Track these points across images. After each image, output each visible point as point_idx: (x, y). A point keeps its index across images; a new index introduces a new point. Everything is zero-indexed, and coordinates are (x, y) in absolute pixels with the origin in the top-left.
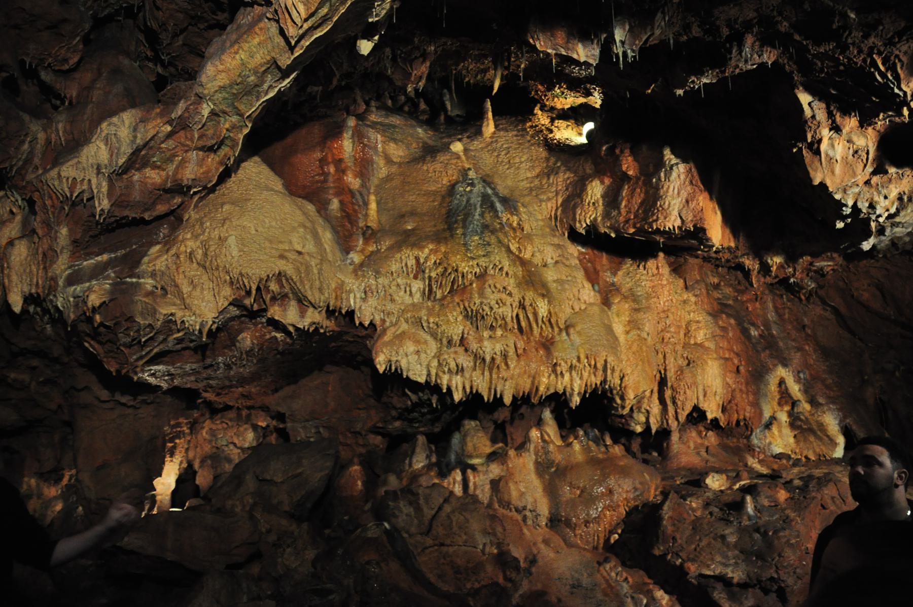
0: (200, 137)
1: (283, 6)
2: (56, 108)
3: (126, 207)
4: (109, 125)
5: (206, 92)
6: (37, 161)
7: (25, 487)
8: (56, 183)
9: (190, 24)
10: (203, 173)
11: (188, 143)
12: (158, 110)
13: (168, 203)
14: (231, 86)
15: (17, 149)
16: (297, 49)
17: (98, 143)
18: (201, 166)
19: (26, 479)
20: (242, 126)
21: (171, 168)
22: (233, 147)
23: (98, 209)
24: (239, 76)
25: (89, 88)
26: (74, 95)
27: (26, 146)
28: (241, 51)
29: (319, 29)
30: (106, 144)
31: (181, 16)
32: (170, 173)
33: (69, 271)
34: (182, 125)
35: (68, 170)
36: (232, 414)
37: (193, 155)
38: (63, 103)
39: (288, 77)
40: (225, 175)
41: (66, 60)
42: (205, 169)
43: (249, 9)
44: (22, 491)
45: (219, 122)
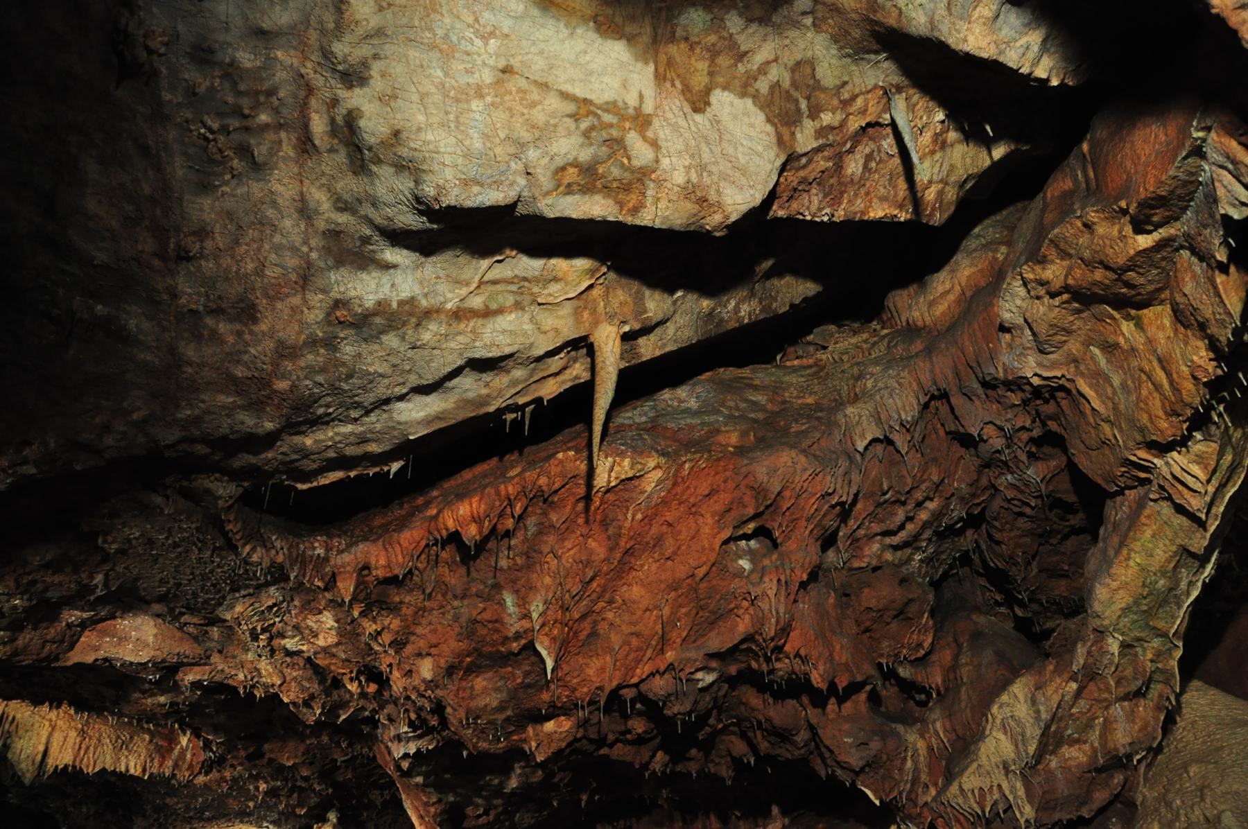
0: (1118, 683)
1: (1169, 477)
2: (923, 704)
3: (1054, 809)
4: (1000, 707)
5: (1106, 622)
6: (924, 777)
8: (960, 801)
9: (1040, 545)
10: (1140, 730)
11: (1105, 695)
12: (1051, 667)
13: (1107, 785)
14: (1136, 603)
15: (901, 770)
16: (1210, 522)
17: (994, 734)
18: (1133, 721)
20: (1170, 650)
21: (1094, 736)
22: (1167, 682)
23: (1022, 821)
24: (1144, 585)
25: (954, 667)
26: (939, 680)
27: (909, 763)
28: (1133, 555)
29: (1230, 484)
30: (1005, 733)
31: (1028, 540)
32: (1096, 744)
34: (1090, 675)
35: (970, 780)
37: (1118, 710)
38: (929, 696)
39: (1209, 561)
40: (1170, 721)
41: (920, 645)
42: (1139, 723)
43: (1119, 499)
45: (1136, 655)
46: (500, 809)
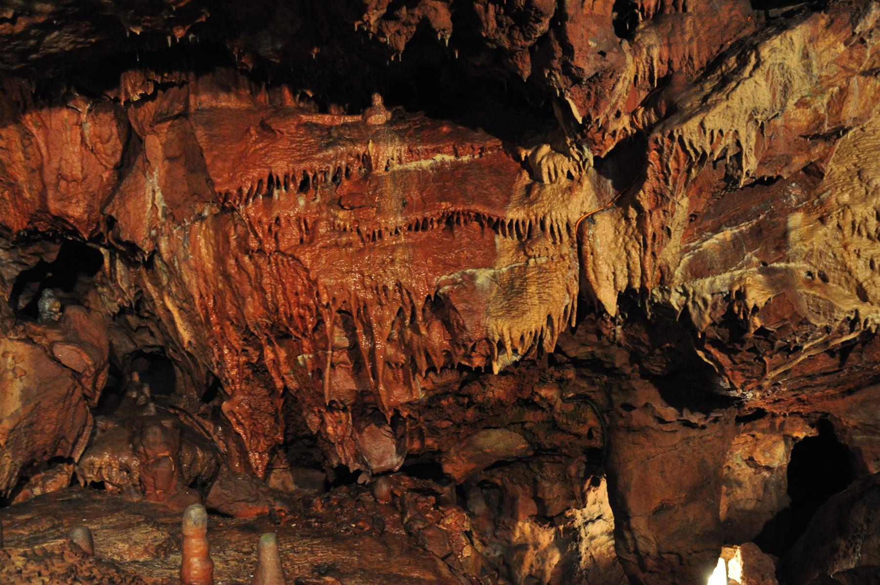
7: (518, 534)
19: (520, 524)
30: (766, 80)
33: (687, 258)
36: (764, 424)
44: (514, 540)
46: (40, 20)
